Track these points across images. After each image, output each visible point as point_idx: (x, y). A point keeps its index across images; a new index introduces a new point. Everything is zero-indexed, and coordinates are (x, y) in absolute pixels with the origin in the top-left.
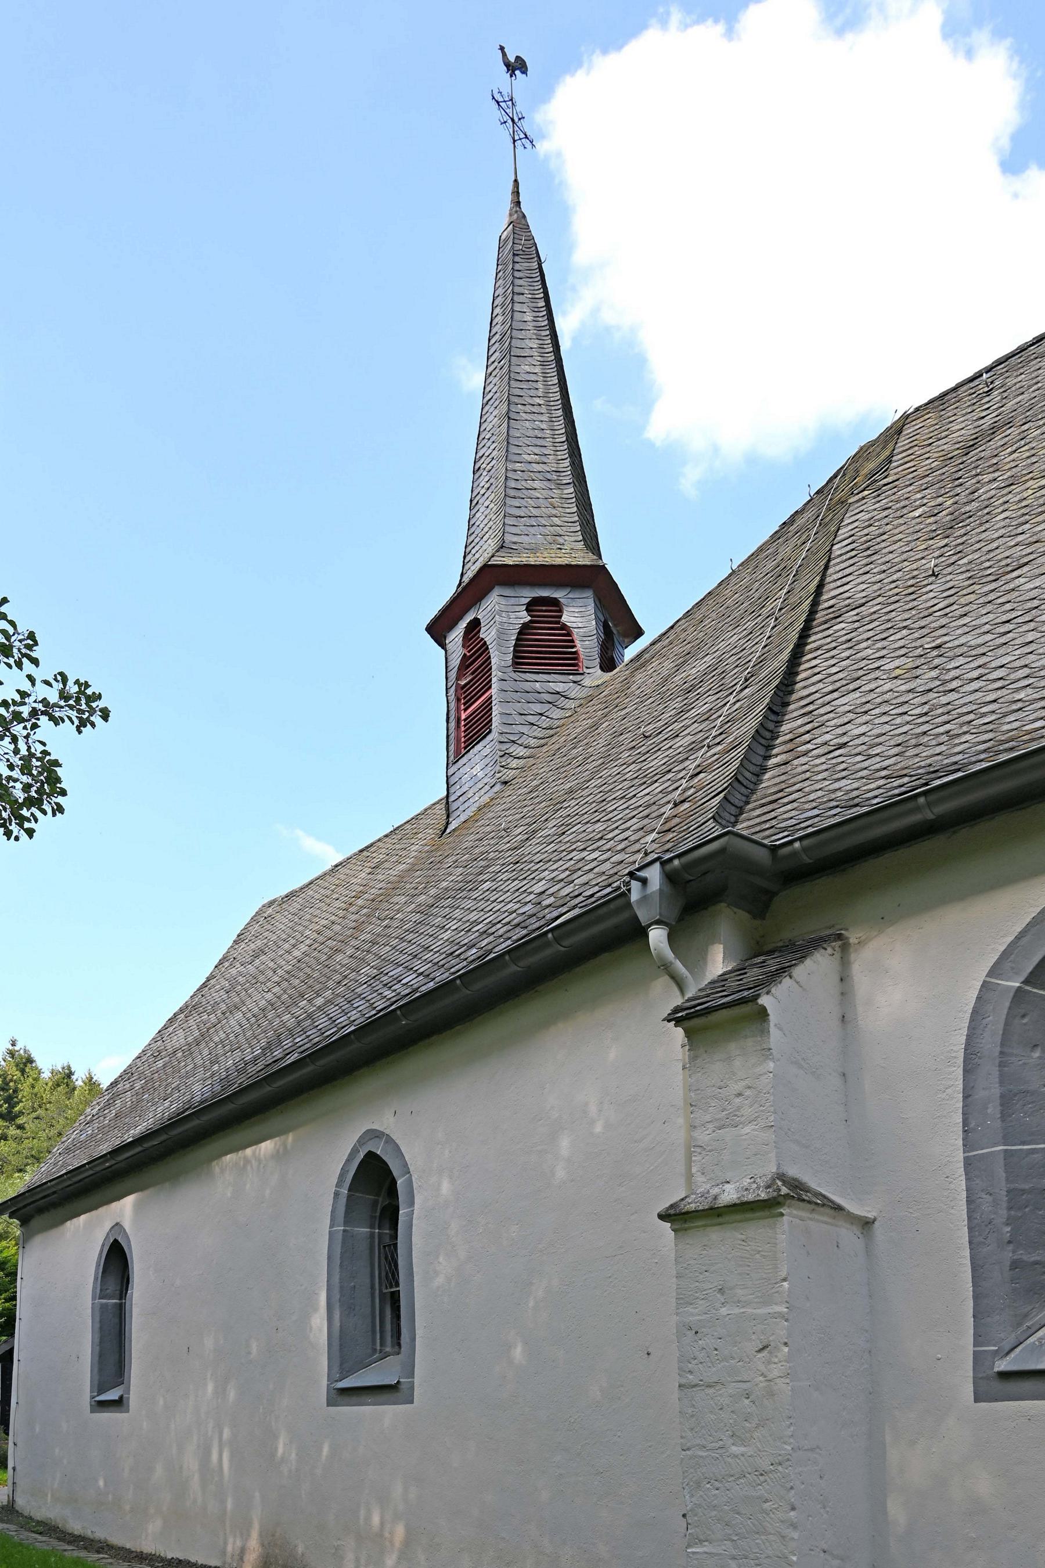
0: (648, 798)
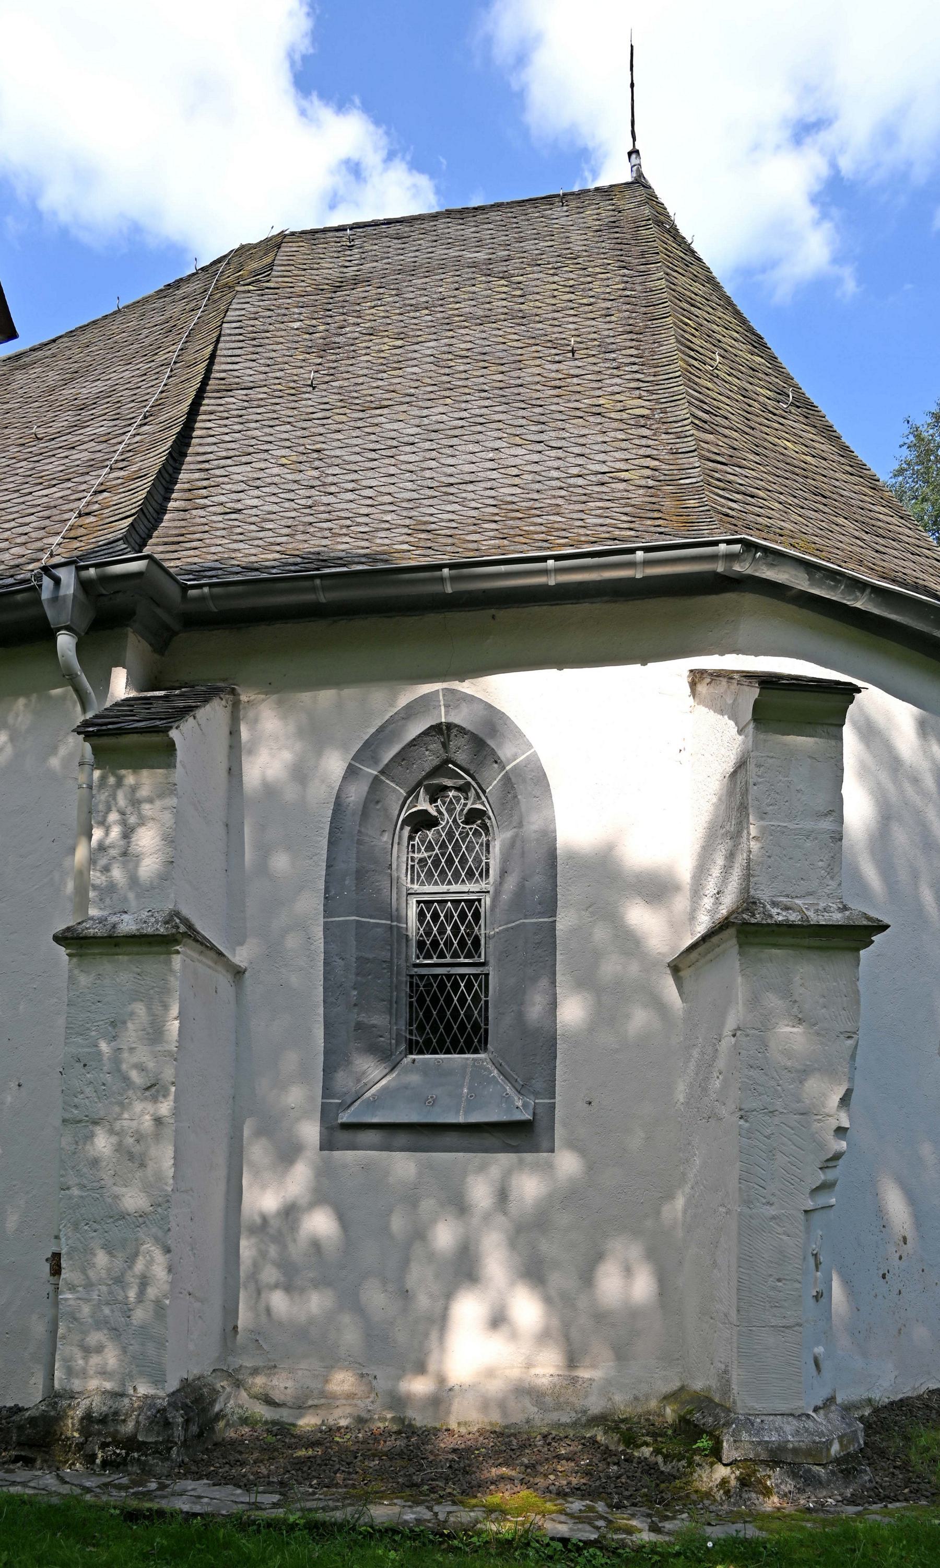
0: (45, 499)
